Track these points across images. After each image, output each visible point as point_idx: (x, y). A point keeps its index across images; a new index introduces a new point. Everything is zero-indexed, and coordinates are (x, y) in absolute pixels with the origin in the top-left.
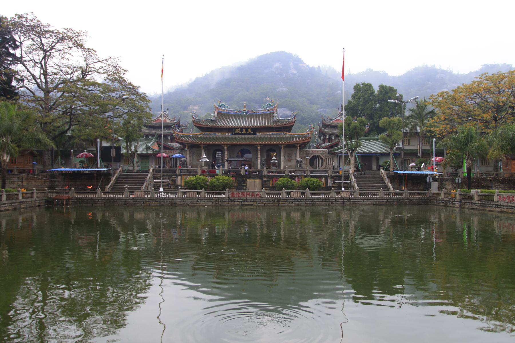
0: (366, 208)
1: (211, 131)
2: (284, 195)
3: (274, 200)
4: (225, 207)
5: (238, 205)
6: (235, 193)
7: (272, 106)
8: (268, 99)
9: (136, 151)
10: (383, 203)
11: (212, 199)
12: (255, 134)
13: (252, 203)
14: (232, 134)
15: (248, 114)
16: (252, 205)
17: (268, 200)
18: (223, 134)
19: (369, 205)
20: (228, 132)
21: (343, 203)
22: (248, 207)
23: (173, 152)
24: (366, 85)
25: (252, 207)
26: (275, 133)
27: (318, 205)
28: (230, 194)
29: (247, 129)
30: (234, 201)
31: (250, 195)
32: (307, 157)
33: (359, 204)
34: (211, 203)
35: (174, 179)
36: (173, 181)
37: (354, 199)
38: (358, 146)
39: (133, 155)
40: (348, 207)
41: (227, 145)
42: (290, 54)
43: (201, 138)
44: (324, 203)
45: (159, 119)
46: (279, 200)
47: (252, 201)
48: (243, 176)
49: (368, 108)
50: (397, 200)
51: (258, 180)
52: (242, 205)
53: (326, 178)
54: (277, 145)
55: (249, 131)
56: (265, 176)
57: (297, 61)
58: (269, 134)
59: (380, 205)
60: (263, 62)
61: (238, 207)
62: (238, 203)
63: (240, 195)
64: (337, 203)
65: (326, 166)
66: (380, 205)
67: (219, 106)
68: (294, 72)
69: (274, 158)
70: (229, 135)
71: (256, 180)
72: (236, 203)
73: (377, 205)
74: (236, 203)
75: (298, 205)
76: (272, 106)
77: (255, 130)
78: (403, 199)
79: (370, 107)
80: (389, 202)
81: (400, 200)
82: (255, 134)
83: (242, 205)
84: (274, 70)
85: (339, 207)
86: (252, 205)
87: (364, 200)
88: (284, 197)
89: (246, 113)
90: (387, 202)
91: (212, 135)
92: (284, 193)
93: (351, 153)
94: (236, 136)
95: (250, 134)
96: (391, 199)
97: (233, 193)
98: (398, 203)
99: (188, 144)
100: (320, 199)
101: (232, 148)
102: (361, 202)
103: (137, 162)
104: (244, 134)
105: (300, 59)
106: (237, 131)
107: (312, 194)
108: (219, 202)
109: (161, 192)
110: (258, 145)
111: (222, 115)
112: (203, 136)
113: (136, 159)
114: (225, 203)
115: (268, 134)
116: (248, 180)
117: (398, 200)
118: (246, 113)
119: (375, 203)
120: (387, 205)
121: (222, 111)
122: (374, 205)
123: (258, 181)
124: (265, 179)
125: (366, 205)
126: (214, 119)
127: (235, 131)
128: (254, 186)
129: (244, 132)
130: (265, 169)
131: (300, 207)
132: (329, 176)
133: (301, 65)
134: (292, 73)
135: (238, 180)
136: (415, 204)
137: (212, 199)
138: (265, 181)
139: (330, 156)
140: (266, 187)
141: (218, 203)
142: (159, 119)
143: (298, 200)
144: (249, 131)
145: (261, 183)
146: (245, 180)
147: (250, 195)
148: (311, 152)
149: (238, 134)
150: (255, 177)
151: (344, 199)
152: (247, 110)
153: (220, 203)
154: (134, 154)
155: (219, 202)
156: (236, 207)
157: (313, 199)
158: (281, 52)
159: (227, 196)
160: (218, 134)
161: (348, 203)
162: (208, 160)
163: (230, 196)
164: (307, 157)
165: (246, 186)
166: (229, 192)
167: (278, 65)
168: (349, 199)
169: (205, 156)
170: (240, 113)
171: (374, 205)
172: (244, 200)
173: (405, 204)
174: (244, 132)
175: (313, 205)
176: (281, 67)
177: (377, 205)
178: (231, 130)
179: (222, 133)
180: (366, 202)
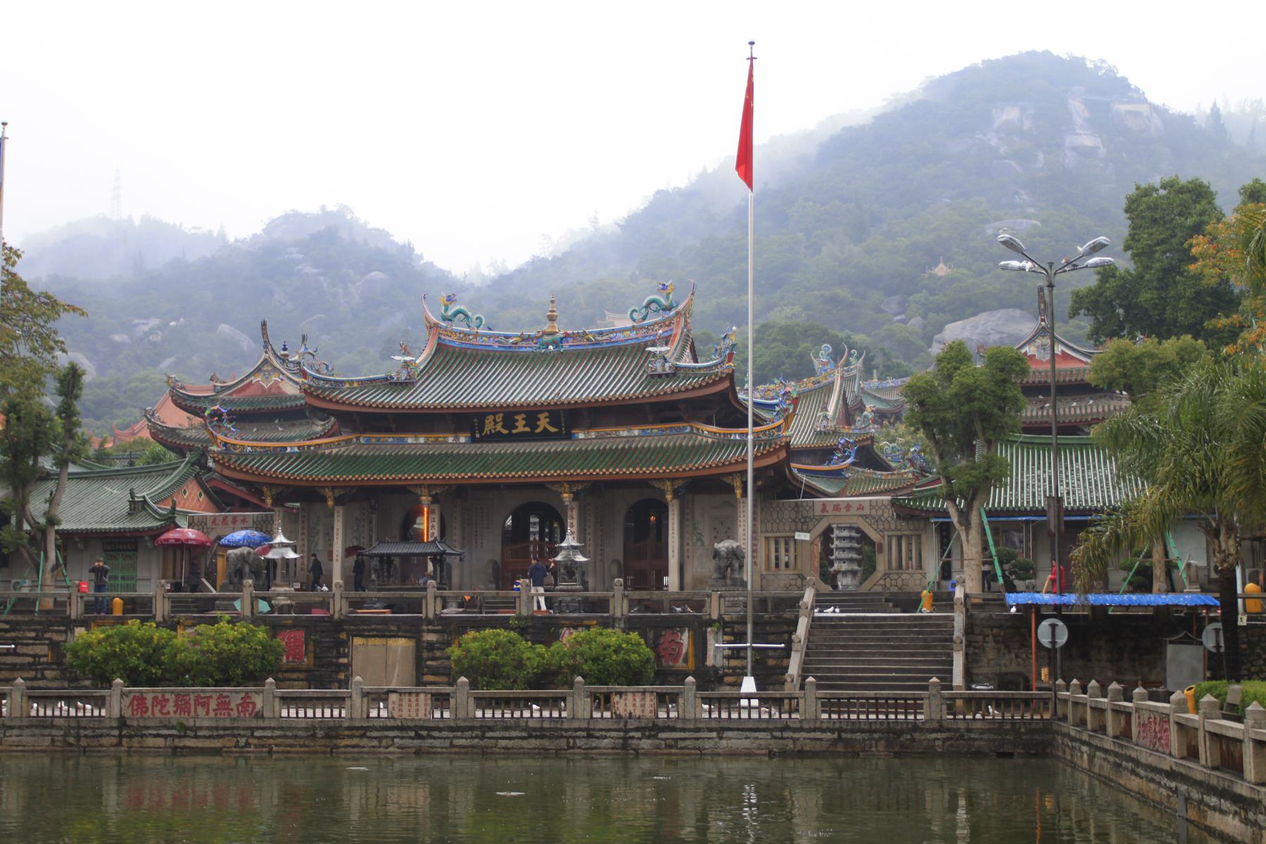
0: (733, 768)
1: (388, 430)
2: (577, 706)
3: (312, 729)
4: (106, 762)
5: (156, 752)
6: (149, 697)
7: (669, 309)
8: (941, 270)
9: (52, 521)
10: (818, 746)
11: (52, 726)
12: (569, 437)
13: (217, 744)
14: (473, 440)
15: (566, 346)
16: (217, 752)
17: (287, 728)
18: (436, 441)
19: (748, 754)
20: (457, 430)
21: (625, 747)
22: (199, 760)
23: (235, 519)
24: (1182, 190)
25: (217, 760)
26: (655, 429)
27: (508, 753)
28: (127, 701)
29: (531, 413)
30: (140, 732)
31: (213, 705)
32: (800, 536)
33: (702, 754)
34: (48, 741)
35: (56, 637)
36: (54, 645)
37: (673, 729)
38: (992, 476)
39: (38, 538)
40: (646, 764)
41: (571, 483)
42: (1075, 66)
43: (336, 458)
44: (534, 743)
45: (254, 379)
46: (333, 731)
47: (217, 732)
48: (338, 625)
49: (1179, 297)
50: (889, 731)
51: (402, 642)
52: (176, 751)
53: (699, 629)
54: (403, 490)
55: (543, 422)
56: (429, 622)
57: (1108, 89)
58: (629, 434)
59: (801, 754)
60: (966, 100)
61: (160, 761)
62: (160, 742)
63: (170, 707)
64: (595, 743)
65: (885, 576)
66: (801, 754)
67: (445, 319)
68: (1087, 141)
69: (570, 540)
70: (458, 442)
71: (392, 642)
72: (150, 742)
73: (784, 754)
74: (150, 742)
75: (418, 753)
76: (669, 309)
77: (570, 417)
78: (915, 727)
79: (1189, 292)
80: (847, 743)
81: (899, 733)
82: (569, 437)
83: (175, 748)
84: (994, 142)
85: (605, 764)
86: (217, 752)
87: (721, 730)
88: (357, 715)
89: (555, 343)
90: (834, 742)
91: (388, 444)
92: (357, 699)
93: (964, 516)
94: (486, 448)
95: (545, 436)
96: (855, 727)
97: (141, 699)
98: (889, 745)
99: (271, 486)
100: (516, 725)
101: (461, 500)
102: (710, 741)
103: (53, 569)
104: (522, 437)
105: (1124, 80)
106: (489, 426)
107: (483, 703)
108: (78, 737)
109: (749, 697)
110: (662, 480)
111: (452, 356)
112: (350, 450)
113: (52, 553)
114: (105, 741)
115: (624, 433)
116: (358, 641)
117: (892, 733)
118: (555, 343)
119: (775, 745)
120: (834, 755)
121: (453, 341)
122: (771, 754)
123: (401, 645)
124: (431, 637)
125: (733, 755)
126: (403, 377)
127: (482, 428)
128: (381, 661)
129: (521, 426)
130: (618, 591)
131: (427, 763)
132: (710, 623)
133: (1123, 108)
134: (1075, 149)
135: (316, 643)
136: (979, 754)
137: (52, 726)
138: (431, 646)
139: (905, 528)
140: (435, 672)
141: (76, 740)
142: (254, 379)
143: (419, 730)
144: (543, 422)
145: (411, 655)
146: (344, 643)
147: (213, 705)
148: (818, 512)
149: (495, 437)
150: (383, 630)
151: (624, 725)
152: (561, 334)
153: (83, 742)
154: (44, 532)
155: (78, 737)
156: (149, 761)
157: (485, 728)
158: (1032, 54)
159: (116, 713)
160: (416, 442)
161: (646, 744)
162: (291, 555)
163: (127, 713)
164: (800, 536)
165: (347, 666)
166: (123, 695)
167: (1011, 114)
168: (653, 729)
169: (280, 538)
170: (528, 348)
171: (771, 754)
172: (184, 731)
173: (929, 754)
174: (521, 426)
175: (485, 753)
176: (1027, 125)
177: (784, 754)
178: (465, 420)
179: (432, 437)
180: (734, 741)
